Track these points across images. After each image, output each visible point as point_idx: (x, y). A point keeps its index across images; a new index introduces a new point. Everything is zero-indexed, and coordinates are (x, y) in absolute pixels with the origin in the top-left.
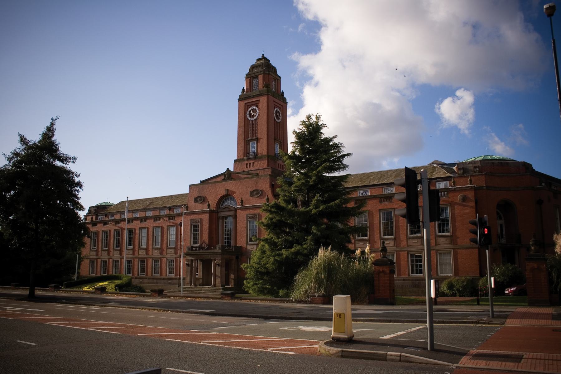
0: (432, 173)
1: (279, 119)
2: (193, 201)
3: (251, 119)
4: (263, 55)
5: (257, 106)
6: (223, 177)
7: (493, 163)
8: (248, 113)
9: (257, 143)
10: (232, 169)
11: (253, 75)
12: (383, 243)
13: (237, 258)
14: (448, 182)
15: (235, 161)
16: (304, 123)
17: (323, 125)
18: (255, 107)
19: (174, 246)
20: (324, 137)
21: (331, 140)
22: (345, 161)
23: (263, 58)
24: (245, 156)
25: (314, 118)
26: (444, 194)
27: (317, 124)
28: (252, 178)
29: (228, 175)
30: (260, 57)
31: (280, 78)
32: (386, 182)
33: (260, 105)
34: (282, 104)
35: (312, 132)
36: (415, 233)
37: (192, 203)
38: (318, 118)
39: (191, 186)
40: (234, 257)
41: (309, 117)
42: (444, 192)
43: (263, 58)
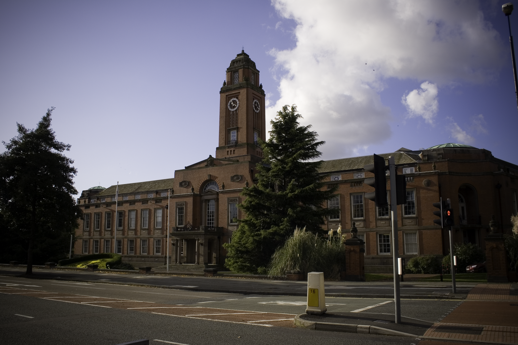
0: (399, 159)
1: (258, 110)
2: (178, 186)
3: (232, 110)
4: (243, 51)
5: (237, 98)
6: (206, 164)
7: (455, 150)
8: (229, 104)
9: (237, 132)
10: (214, 156)
11: (234, 69)
12: (354, 224)
13: (219, 238)
14: (414, 168)
15: (217, 148)
16: (280, 113)
17: (298, 116)
18: (235, 99)
19: (160, 227)
20: (299, 126)
21: (305, 129)
22: (319, 148)
23: (243, 53)
24: (226, 144)
25: (290, 109)
26: (410, 179)
27: (293, 115)
28: (232, 164)
29: (210, 162)
30: (240, 52)
31: (259, 72)
32: (356, 167)
33: (240, 97)
34: (261, 96)
35: (288, 121)
36: (383, 215)
37: (177, 187)
38: (293, 109)
39: (176, 172)
40: (216, 237)
41: (285, 108)
42: (410, 177)
43: (243, 53)
